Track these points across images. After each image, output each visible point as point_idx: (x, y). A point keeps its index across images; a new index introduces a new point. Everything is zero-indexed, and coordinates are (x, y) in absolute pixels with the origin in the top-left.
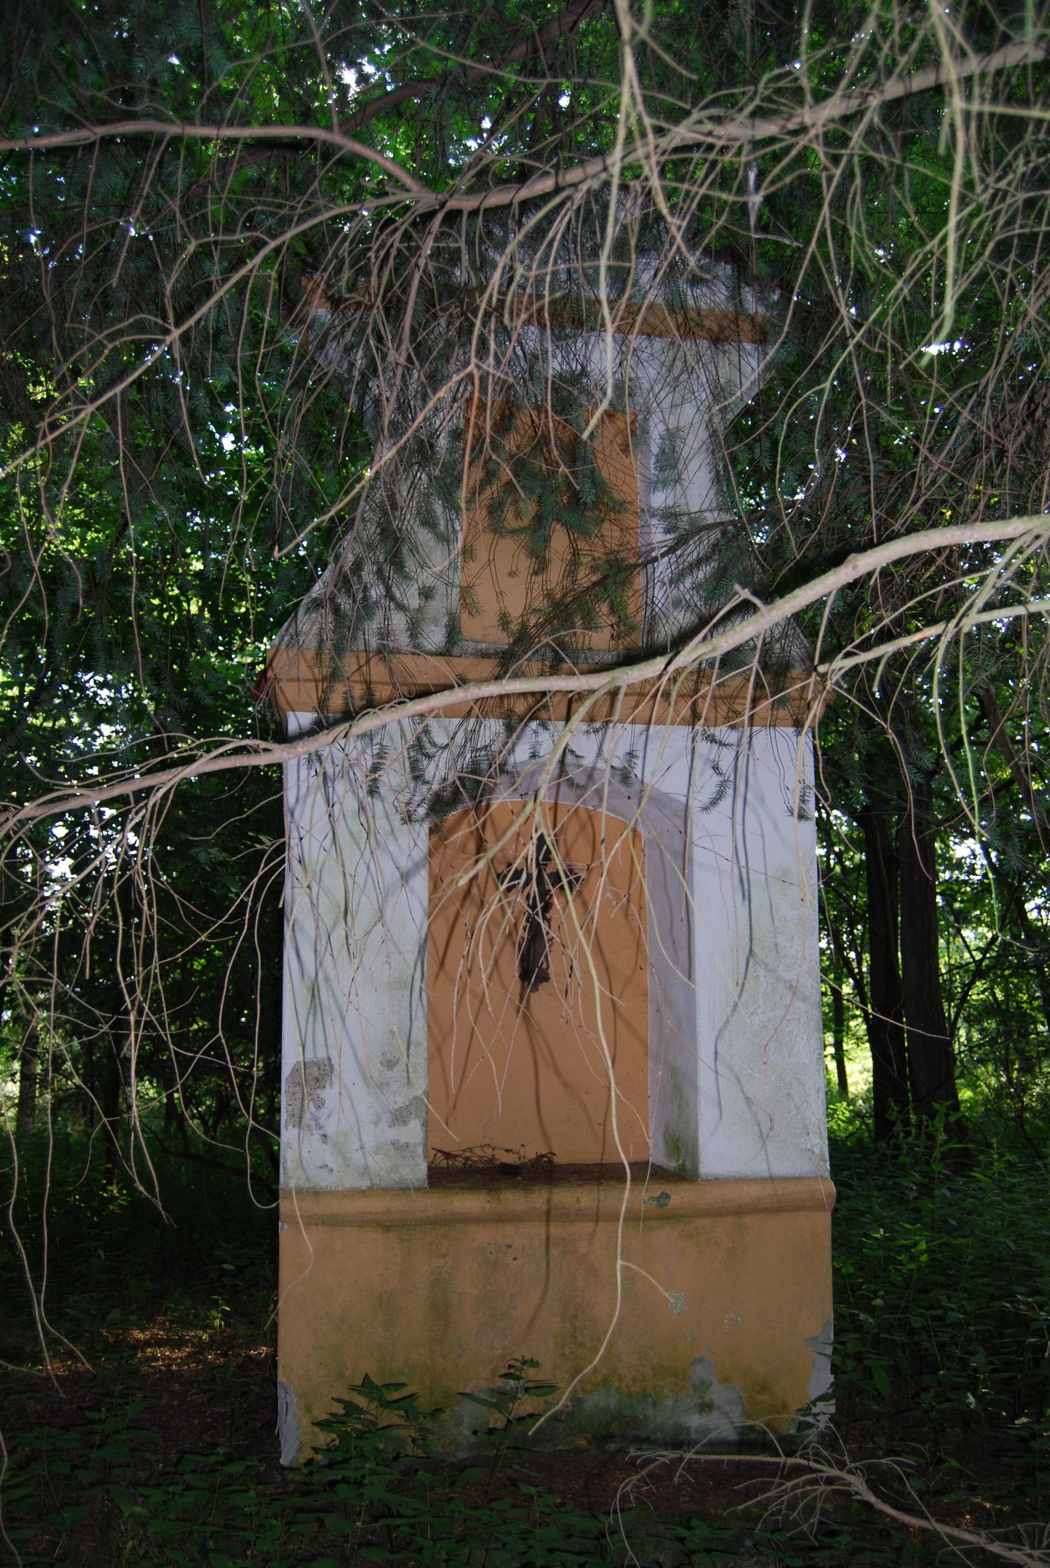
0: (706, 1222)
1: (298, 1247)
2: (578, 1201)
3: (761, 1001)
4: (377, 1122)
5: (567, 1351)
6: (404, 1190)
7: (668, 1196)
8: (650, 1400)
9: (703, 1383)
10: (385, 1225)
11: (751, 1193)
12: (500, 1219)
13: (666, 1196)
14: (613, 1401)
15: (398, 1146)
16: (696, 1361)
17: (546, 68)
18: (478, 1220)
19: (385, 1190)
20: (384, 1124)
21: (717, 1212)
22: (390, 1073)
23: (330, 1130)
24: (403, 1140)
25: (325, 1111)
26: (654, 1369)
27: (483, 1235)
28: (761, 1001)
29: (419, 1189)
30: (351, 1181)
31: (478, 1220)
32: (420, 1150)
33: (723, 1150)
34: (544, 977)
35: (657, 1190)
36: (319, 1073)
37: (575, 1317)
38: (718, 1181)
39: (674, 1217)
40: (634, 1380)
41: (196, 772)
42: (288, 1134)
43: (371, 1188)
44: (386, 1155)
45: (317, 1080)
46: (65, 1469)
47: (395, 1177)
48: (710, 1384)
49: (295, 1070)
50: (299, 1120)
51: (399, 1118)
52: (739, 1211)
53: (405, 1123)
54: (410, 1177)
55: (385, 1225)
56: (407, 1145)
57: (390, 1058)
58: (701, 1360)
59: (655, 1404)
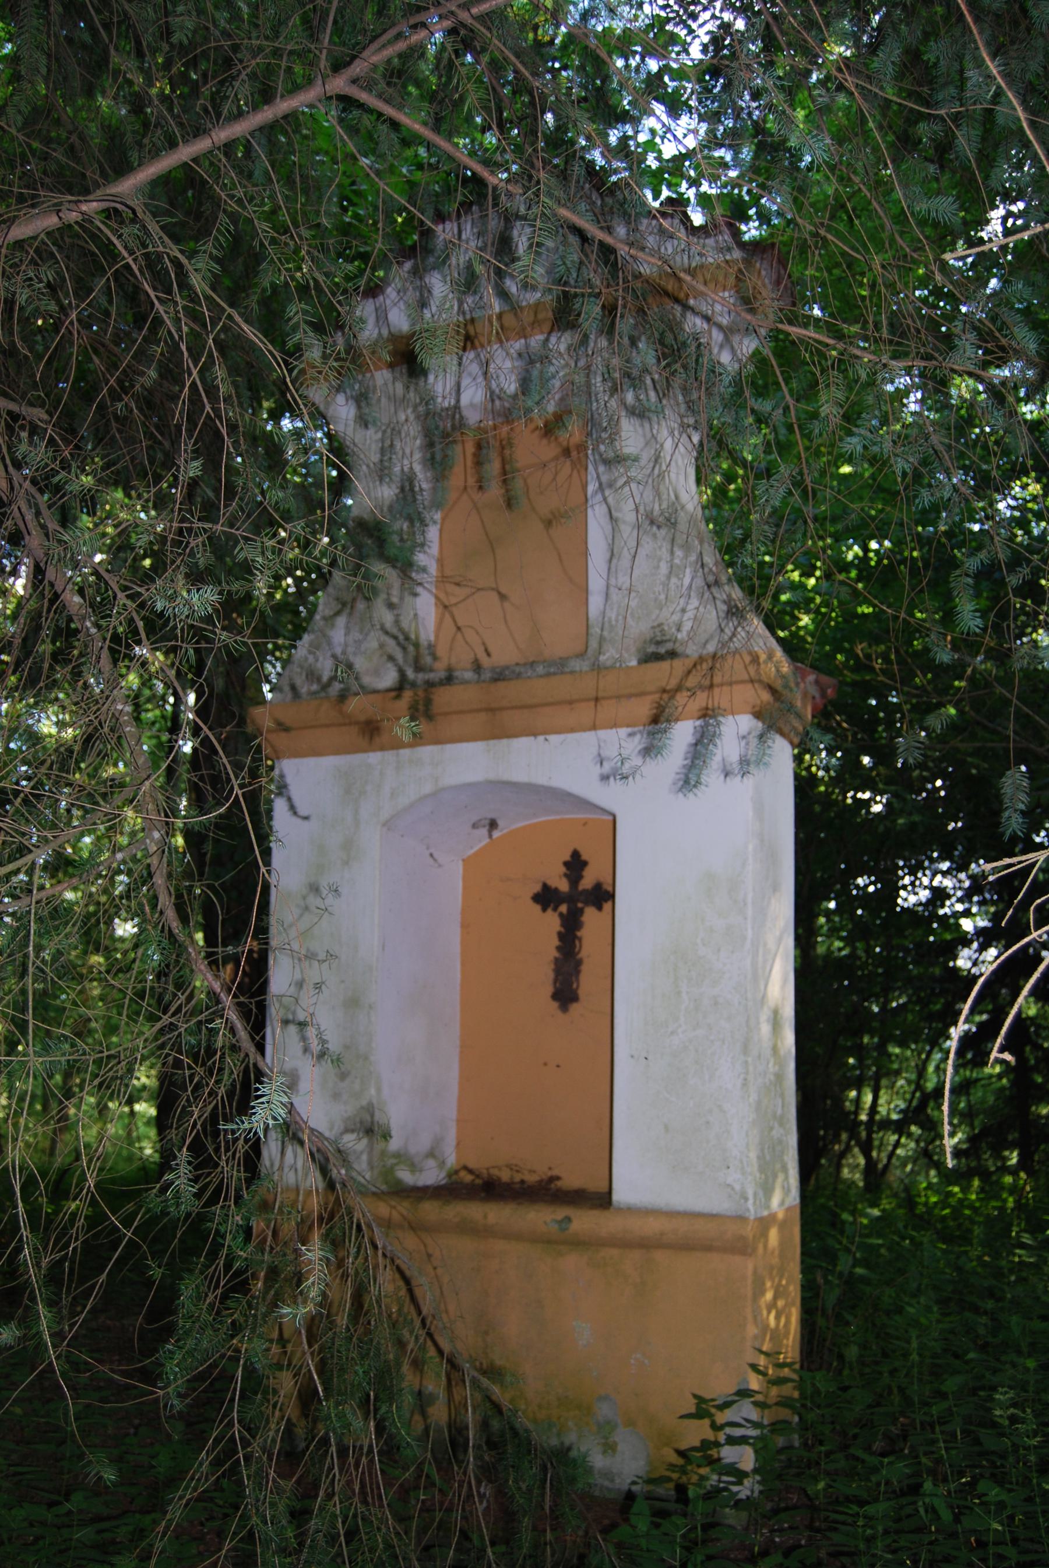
0: (615, 1252)
2: (485, 1217)
8: (554, 1430)
11: (652, 1227)
13: (568, 1219)
34: (575, 998)
35: (561, 1212)
37: (486, 1333)
38: (631, 1211)
39: (579, 1243)
52: (646, 1244)
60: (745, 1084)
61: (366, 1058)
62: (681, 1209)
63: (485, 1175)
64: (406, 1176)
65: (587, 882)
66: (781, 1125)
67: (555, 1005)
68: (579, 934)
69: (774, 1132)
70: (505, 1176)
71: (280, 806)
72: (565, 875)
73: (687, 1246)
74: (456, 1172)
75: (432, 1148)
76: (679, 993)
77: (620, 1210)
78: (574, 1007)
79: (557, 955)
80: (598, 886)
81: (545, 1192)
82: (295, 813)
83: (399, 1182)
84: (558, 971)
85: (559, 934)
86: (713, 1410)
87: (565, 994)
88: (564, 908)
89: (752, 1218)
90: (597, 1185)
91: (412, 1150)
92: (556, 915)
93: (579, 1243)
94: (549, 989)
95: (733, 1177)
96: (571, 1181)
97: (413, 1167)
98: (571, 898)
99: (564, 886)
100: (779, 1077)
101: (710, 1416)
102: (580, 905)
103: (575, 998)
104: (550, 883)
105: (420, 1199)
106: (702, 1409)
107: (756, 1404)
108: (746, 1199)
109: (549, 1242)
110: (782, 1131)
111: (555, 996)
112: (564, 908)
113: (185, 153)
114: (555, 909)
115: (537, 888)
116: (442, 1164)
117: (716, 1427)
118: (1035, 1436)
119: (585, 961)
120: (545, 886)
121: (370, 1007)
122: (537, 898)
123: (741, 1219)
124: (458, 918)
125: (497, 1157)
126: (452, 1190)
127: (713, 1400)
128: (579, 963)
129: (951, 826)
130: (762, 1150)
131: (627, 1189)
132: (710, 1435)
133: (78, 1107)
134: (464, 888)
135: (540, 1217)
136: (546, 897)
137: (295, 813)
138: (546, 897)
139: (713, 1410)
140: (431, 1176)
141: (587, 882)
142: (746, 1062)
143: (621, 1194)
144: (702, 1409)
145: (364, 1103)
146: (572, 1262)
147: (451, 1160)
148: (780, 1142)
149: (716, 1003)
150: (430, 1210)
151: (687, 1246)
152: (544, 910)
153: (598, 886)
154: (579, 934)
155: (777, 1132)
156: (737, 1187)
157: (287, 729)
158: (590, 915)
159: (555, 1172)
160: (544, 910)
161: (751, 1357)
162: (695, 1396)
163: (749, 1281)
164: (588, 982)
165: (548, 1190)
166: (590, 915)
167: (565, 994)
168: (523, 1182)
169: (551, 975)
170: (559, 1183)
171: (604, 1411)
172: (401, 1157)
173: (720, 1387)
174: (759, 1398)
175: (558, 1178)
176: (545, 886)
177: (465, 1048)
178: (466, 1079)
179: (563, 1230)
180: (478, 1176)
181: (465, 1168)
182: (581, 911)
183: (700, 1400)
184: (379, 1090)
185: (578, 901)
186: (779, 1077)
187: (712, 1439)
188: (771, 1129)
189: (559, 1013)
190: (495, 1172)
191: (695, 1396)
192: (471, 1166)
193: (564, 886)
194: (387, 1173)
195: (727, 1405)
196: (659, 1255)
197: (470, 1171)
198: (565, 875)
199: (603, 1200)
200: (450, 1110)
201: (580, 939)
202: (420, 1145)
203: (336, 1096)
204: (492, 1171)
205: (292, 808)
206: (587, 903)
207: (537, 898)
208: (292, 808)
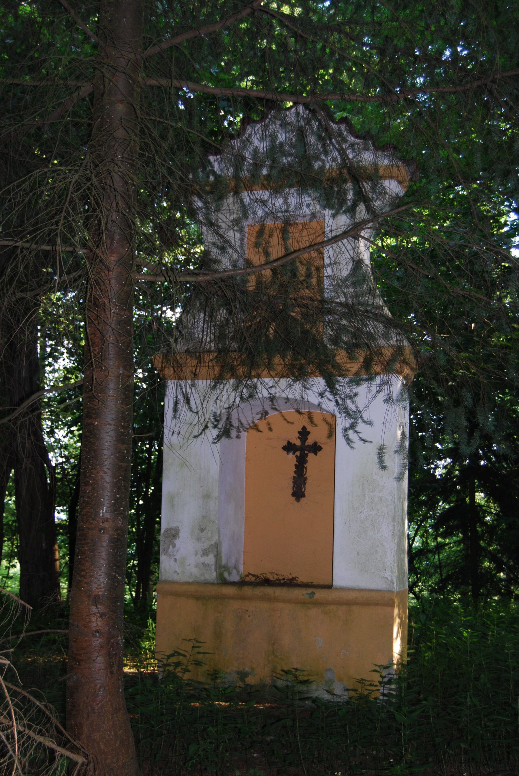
2: (275, 592)
3: (366, 506)
4: (196, 554)
5: (270, 659)
6: (206, 583)
7: (314, 593)
10: (198, 598)
11: (352, 596)
12: (243, 598)
13: (314, 593)
16: (327, 670)
18: (233, 598)
19: (198, 583)
20: (199, 556)
21: (339, 603)
23: (178, 557)
24: (206, 562)
25: (176, 548)
27: (236, 605)
28: (366, 506)
29: (213, 584)
30: (184, 579)
31: (233, 598)
32: (213, 567)
33: (346, 574)
34: (303, 496)
35: (310, 591)
36: (174, 534)
37: (274, 644)
38: (341, 589)
39: (318, 604)
41: (166, 407)
43: (193, 582)
45: (174, 536)
47: (202, 578)
48: (334, 681)
50: (166, 552)
51: (205, 553)
52: (349, 603)
53: (208, 555)
55: (198, 598)
56: (208, 565)
57: (202, 527)
58: (329, 670)
60: (393, 534)
65: (310, 442)
72: (299, 438)
73: (366, 604)
76: (364, 495)
77: (336, 589)
78: (302, 500)
79: (295, 475)
80: (315, 444)
83: (225, 579)
85: (296, 465)
87: (298, 494)
88: (298, 453)
92: (294, 456)
94: (291, 491)
95: (388, 574)
99: (298, 443)
102: (306, 452)
103: (303, 496)
104: (291, 441)
108: (393, 583)
111: (293, 495)
115: (285, 443)
123: (391, 592)
126: (242, 583)
128: (306, 479)
129: (182, 107)
136: (289, 447)
138: (289, 447)
141: (310, 442)
142: (394, 525)
145: (213, 543)
146: (314, 612)
149: (381, 500)
150: (248, 591)
151: (366, 604)
153: (315, 444)
156: (389, 578)
158: (311, 457)
164: (309, 488)
165: (297, 584)
166: (311, 457)
167: (298, 494)
169: (292, 485)
179: (311, 598)
182: (307, 455)
189: (295, 502)
193: (298, 443)
197: (253, 576)
198: (299, 438)
199: (330, 587)
201: (306, 468)
202: (232, 563)
203: (199, 539)
206: (310, 452)
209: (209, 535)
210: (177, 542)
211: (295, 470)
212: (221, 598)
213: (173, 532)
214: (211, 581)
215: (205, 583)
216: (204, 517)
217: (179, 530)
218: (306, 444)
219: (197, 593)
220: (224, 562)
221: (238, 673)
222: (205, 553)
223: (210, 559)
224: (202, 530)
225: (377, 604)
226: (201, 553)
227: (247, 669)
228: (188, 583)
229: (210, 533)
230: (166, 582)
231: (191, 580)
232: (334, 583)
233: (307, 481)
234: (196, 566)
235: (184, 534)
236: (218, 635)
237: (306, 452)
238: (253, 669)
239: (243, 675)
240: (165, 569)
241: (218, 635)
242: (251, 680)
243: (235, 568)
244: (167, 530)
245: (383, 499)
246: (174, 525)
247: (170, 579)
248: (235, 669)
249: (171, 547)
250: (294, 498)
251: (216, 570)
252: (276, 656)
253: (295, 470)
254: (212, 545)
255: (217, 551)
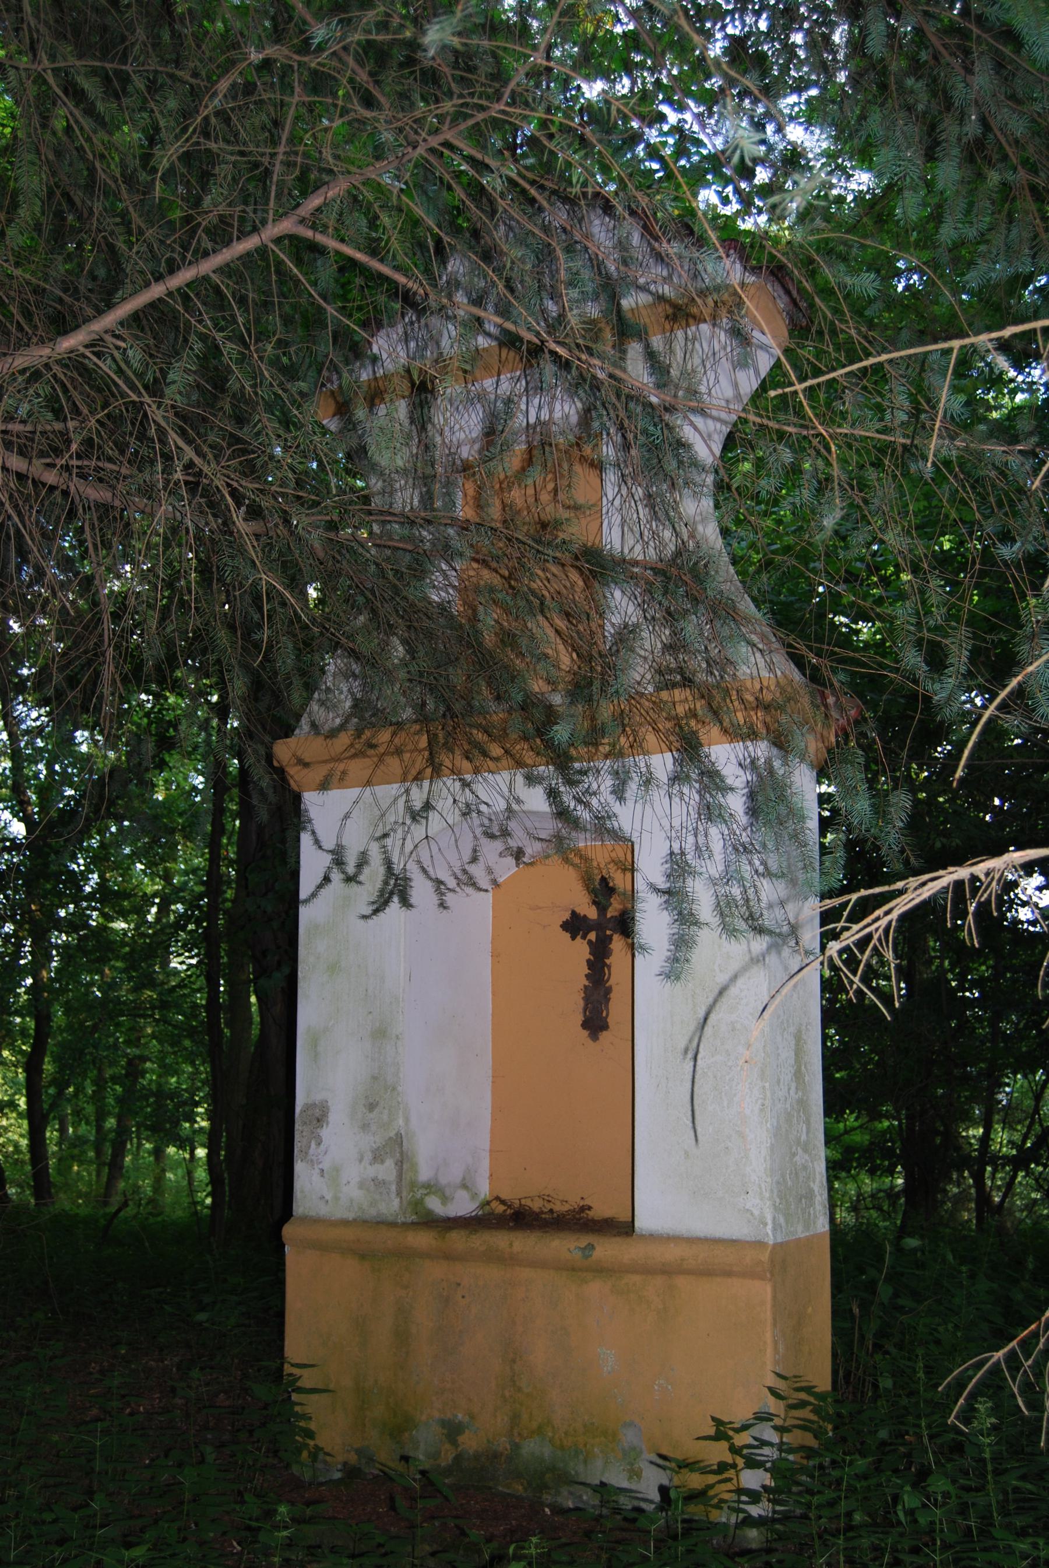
0: (637, 1278)
1: (299, 1266)
2: (511, 1245)
5: (507, 1394)
6: (381, 1223)
8: (581, 1457)
9: (634, 1449)
11: (672, 1253)
12: (449, 1257)
13: (591, 1247)
14: (547, 1451)
15: (378, 1183)
17: (482, 314)
19: (365, 1222)
21: (648, 1270)
22: (371, 1115)
26: (585, 1426)
33: (662, 1204)
34: (605, 1027)
35: (584, 1240)
36: (320, 1116)
37: (514, 1361)
39: (602, 1271)
40: (566, 1433)
42: (299, 1167)
43: (355, 1220)
44: (368, 1190)
46: (249, 1486)
47: (373, 1212)
49: (303, 1111)
51: (378, 1157)
52: (668, 1271)
53: (382, 1162)
54: (385, 1211)
56: (384, 1182)
59: (585, 1462)
61: (394, 1089)
62: (702, 1235)
63: (517, 1205)
64: (434, 1204)
66: (806, 1150)
67: (585, 1033)
68: (607, 961)
69: (797, 1158)
70: (536, 1205)
71: (306, 839)
74: (488, 1203)
75: (464, 1179)
77: (642, 1236)
78: (604, 1035)
81: (579, 1222)
82: (320, 847)
83: (429, 1212)
84: (587, 1000)
85: (588, 961)
86: (731, 1433)
87: (595, 1023)
88: (592, 936)
89: (771, 1242)
90: (625, 1217)
91: (443, 1181)
93: (602, 1271)
94: (580, 1018)
96: (601, 1210)
97: (445, 1199)
98: (599, 926)
99: (592, 913)
100: (802, 1104)
101: (728, 1438)
102: (608, 932)
103: (605, 1027)
104: (578, 910)
105: (450, 1229)
106: (721, 1431)
107: (776, 1428)
108: (766, 1224)
109: (573, 1269)
110: (806, 1157)
111: (585, 1025)
112: (592, 936)
113: (157, 291)
114: (584, 937)
115: (567, 916)
116: (474, 1196)
117: (735, 1450)
118: (989, 1435)
119: (614, 988)
120: (574, 913)
121: (397, 1037)
122: (566, 926)
124: (489, 947)
125: (527, 1188)
127: (731, 1423)
128: (609, 990)
130: (783, 1176)
131: (650, 1216)
132: (728, 1458)
133: (136, 1156)
134: (494, 917)
135: (564, 1246)
136: (575, 925)
137: (320, 847)
138: (575, 925)
139: (731, 1433)
140: (463, 1206)
142: (764, 1087)
143: (644, 1222)
144: (721, 1431)
145: (392, 1134)
146: (595, 1288)
147: (484, 1190)
148: (805, 1168)
150: (458, 1240)
151: (706, 1272)
152: (573, 938)
154: (607, 961)
155: (801, 1158)
156: (756, 1212)
157: (306, 765)
158: (618, 944)
159: (587, 1202)
160: (573, 938)
161: (771, 1381)
162: (713, 1419)
163: (769, 1306)
165: (561, 1221)
167: (595, 1023)
168: (551, 1211)
169: (582, 1003)
170: (591, 1213)
171: (629, 1437)
172: (431, 1188)
173: (741, 1413)
174: (778, 1421)
175: (590, 1208)
176: (574, 913)
177: (497, 1078)
178: (497, 1110)
180: (509, 1207)
181: (497, 1198)
182: (610, 938)
183: (718, 1422)
184: (407, 1120)
185: (607, 928)
186: (802, 1104)
187: (731, 1461)
188: (794, 1155)
190: (528, 1202)
191: (713, 1419)
192: (503, 1197)
193: (592, 913)
194: (417, 1205)
195: (745, 1428)
196: (681, 1281)
197: (503, 1202)
199: (626, 1228)
200: (483, 1140)
201: (609, 967)
202: (452, 1175)
203: (365, 1127)
204: (523, 1202)
205: (317, 842)
207: (566, 926)
208: (317, 842)
209: (385, 1117)
210: (325, 1133)
211: (587, 971)
212: (405, 1255)
213: (317, 1113)
214: (390, 1219)
215: (378, 1223)
216: (375, 1078)
217: (328, 1108)
218: (609, 915)
219: (370, 1244)
220: (424, 1174)
221: (444, 1423)
222: (378, 1157)
223: (387, 1170)
224: (371, 1107)
225: (728, 1274)
226: (369, 1156)
227: (460, 1416)
228: (345, 1223)
229: (386, 1111)
230: (306, 1219)
231: (350, 1216)
232: (637, 1224)
233: (612, 995)
234: (361, 1185)
235: (338, 1117)
236: (402, 1337)
237: (608, 932)
238: (472, 1417)
239: (453, 1430)
240: (302, 1192)
241: (402, 1337)
242: (470, 1442)
243: (464, 1186)
244: (308, 1107)
245: (738, 1026)
246: (318, 1097)
247: (313, 1213)
248: (436, 1415)
249: (313, 1145)
250: (586, 1033)
251: (399, 1194)
252: (520, 1389)
253: (587, 971)
254: (390, 1138)
255: (402, 1153)
